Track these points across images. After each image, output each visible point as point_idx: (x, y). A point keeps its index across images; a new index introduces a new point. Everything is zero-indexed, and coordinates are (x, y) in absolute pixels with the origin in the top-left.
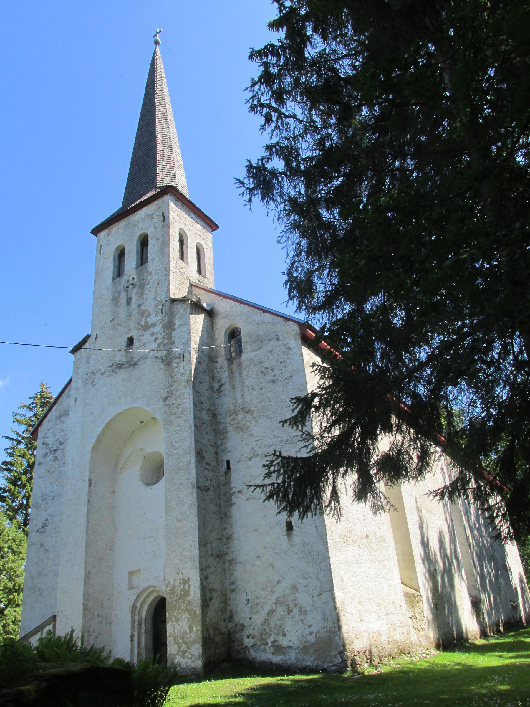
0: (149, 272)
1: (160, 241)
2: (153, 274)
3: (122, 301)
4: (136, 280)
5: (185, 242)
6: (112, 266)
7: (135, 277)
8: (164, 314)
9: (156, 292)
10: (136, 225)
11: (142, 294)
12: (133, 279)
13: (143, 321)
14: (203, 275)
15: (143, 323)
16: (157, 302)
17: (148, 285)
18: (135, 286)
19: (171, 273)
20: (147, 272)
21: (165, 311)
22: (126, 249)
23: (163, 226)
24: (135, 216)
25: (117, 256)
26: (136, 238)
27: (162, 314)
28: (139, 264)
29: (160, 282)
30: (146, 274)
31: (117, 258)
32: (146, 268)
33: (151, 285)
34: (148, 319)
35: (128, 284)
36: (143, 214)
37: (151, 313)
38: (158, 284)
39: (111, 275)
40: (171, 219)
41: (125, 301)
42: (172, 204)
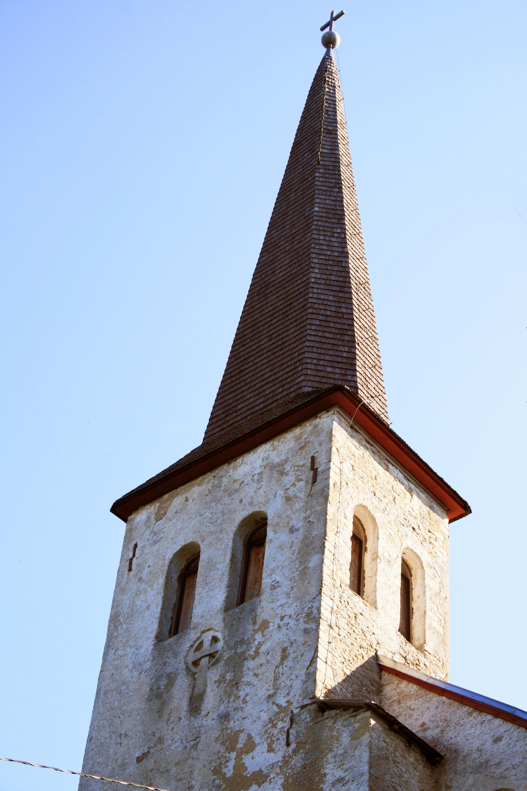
0: (259, 621)
1: (300, 535)
2: (272, 627)
3: (175, 703)
4: (220, 645)
5: (369, 545)
6: (159, 601)
7: (219, 635)
8: (293, 746)
9: (276, 679)
10: (236, 491)
11: (236, 684)
12: (215, 639)
13: (231, 764)
14: (417, 643)
15: (229, 771)
16: (276, 709)
17: (254, 658)
18: (218, 661)
19: (323, 627)
20: (254, 623)
21: (297, 737)
22: (203, 557)
23: (310, 495)
24: (235, 469)
25: (175, 576)
26: (233, 528)
27: (288, 744)
28: (235, 600)
29: (291, 650)
30: (250, 627)
31: (175, 583)
32: (253, 610)
33: (261, 659)
34: (247, 760)
35: (199, 655)
36: (259, 462)
37: (257, 740)
38: (284, 657)
39: (153, 627)
40: (334, 477)
41: (185, 705)
42: (335, 424)
